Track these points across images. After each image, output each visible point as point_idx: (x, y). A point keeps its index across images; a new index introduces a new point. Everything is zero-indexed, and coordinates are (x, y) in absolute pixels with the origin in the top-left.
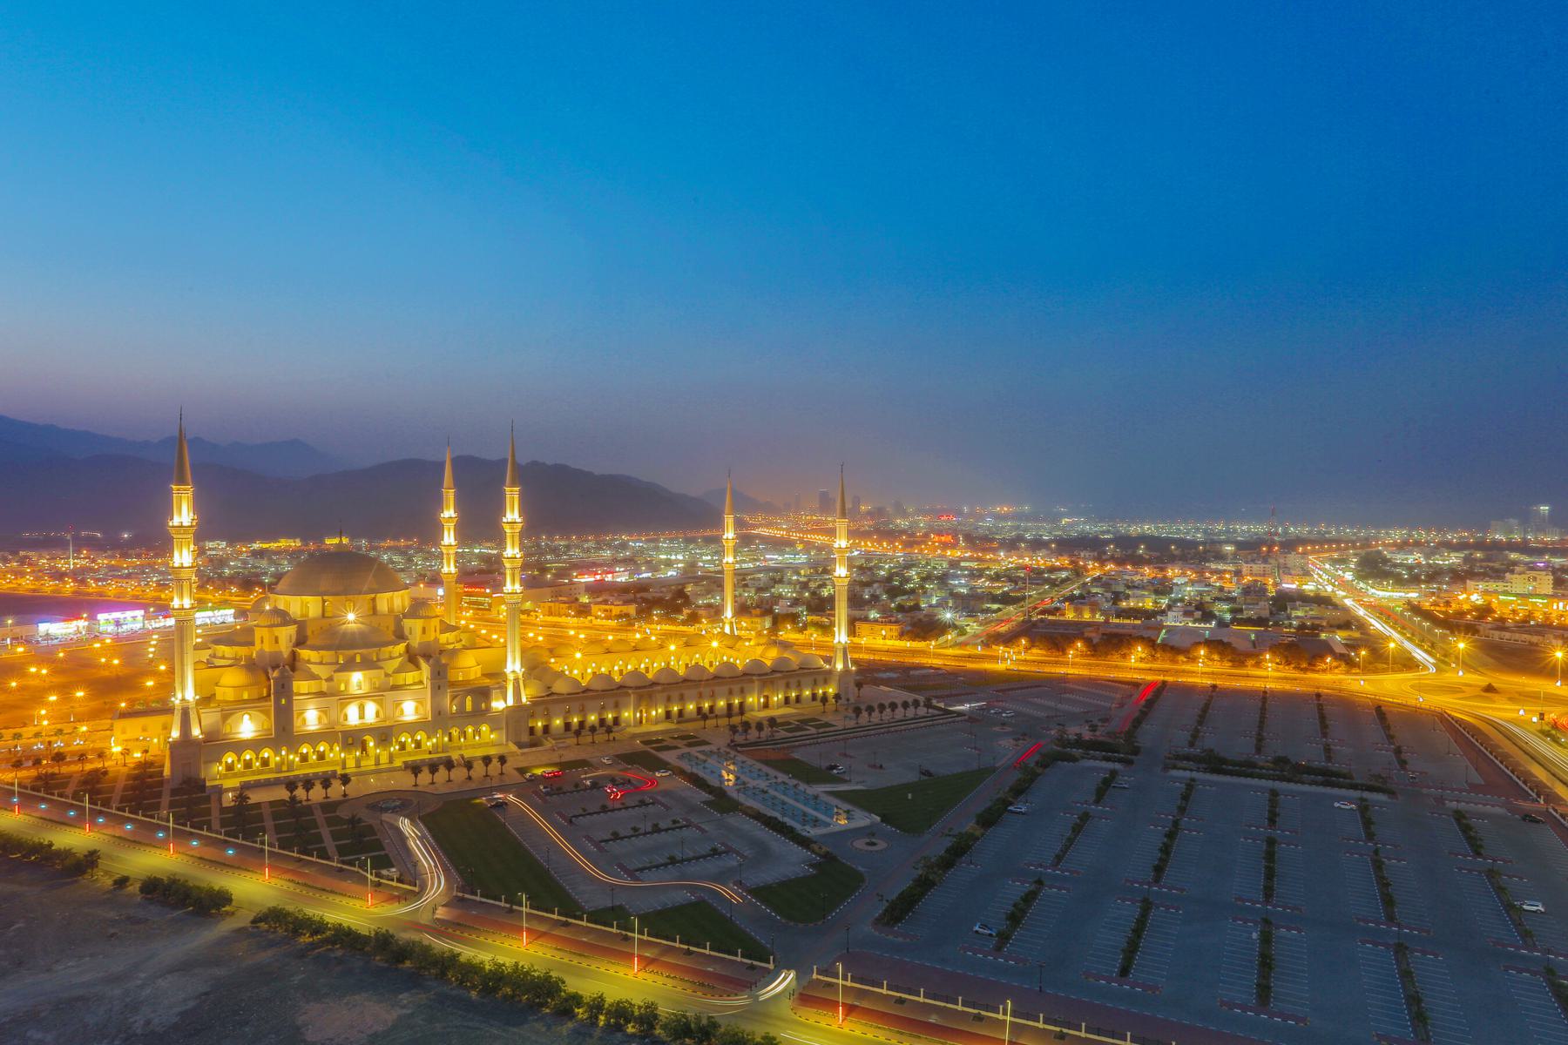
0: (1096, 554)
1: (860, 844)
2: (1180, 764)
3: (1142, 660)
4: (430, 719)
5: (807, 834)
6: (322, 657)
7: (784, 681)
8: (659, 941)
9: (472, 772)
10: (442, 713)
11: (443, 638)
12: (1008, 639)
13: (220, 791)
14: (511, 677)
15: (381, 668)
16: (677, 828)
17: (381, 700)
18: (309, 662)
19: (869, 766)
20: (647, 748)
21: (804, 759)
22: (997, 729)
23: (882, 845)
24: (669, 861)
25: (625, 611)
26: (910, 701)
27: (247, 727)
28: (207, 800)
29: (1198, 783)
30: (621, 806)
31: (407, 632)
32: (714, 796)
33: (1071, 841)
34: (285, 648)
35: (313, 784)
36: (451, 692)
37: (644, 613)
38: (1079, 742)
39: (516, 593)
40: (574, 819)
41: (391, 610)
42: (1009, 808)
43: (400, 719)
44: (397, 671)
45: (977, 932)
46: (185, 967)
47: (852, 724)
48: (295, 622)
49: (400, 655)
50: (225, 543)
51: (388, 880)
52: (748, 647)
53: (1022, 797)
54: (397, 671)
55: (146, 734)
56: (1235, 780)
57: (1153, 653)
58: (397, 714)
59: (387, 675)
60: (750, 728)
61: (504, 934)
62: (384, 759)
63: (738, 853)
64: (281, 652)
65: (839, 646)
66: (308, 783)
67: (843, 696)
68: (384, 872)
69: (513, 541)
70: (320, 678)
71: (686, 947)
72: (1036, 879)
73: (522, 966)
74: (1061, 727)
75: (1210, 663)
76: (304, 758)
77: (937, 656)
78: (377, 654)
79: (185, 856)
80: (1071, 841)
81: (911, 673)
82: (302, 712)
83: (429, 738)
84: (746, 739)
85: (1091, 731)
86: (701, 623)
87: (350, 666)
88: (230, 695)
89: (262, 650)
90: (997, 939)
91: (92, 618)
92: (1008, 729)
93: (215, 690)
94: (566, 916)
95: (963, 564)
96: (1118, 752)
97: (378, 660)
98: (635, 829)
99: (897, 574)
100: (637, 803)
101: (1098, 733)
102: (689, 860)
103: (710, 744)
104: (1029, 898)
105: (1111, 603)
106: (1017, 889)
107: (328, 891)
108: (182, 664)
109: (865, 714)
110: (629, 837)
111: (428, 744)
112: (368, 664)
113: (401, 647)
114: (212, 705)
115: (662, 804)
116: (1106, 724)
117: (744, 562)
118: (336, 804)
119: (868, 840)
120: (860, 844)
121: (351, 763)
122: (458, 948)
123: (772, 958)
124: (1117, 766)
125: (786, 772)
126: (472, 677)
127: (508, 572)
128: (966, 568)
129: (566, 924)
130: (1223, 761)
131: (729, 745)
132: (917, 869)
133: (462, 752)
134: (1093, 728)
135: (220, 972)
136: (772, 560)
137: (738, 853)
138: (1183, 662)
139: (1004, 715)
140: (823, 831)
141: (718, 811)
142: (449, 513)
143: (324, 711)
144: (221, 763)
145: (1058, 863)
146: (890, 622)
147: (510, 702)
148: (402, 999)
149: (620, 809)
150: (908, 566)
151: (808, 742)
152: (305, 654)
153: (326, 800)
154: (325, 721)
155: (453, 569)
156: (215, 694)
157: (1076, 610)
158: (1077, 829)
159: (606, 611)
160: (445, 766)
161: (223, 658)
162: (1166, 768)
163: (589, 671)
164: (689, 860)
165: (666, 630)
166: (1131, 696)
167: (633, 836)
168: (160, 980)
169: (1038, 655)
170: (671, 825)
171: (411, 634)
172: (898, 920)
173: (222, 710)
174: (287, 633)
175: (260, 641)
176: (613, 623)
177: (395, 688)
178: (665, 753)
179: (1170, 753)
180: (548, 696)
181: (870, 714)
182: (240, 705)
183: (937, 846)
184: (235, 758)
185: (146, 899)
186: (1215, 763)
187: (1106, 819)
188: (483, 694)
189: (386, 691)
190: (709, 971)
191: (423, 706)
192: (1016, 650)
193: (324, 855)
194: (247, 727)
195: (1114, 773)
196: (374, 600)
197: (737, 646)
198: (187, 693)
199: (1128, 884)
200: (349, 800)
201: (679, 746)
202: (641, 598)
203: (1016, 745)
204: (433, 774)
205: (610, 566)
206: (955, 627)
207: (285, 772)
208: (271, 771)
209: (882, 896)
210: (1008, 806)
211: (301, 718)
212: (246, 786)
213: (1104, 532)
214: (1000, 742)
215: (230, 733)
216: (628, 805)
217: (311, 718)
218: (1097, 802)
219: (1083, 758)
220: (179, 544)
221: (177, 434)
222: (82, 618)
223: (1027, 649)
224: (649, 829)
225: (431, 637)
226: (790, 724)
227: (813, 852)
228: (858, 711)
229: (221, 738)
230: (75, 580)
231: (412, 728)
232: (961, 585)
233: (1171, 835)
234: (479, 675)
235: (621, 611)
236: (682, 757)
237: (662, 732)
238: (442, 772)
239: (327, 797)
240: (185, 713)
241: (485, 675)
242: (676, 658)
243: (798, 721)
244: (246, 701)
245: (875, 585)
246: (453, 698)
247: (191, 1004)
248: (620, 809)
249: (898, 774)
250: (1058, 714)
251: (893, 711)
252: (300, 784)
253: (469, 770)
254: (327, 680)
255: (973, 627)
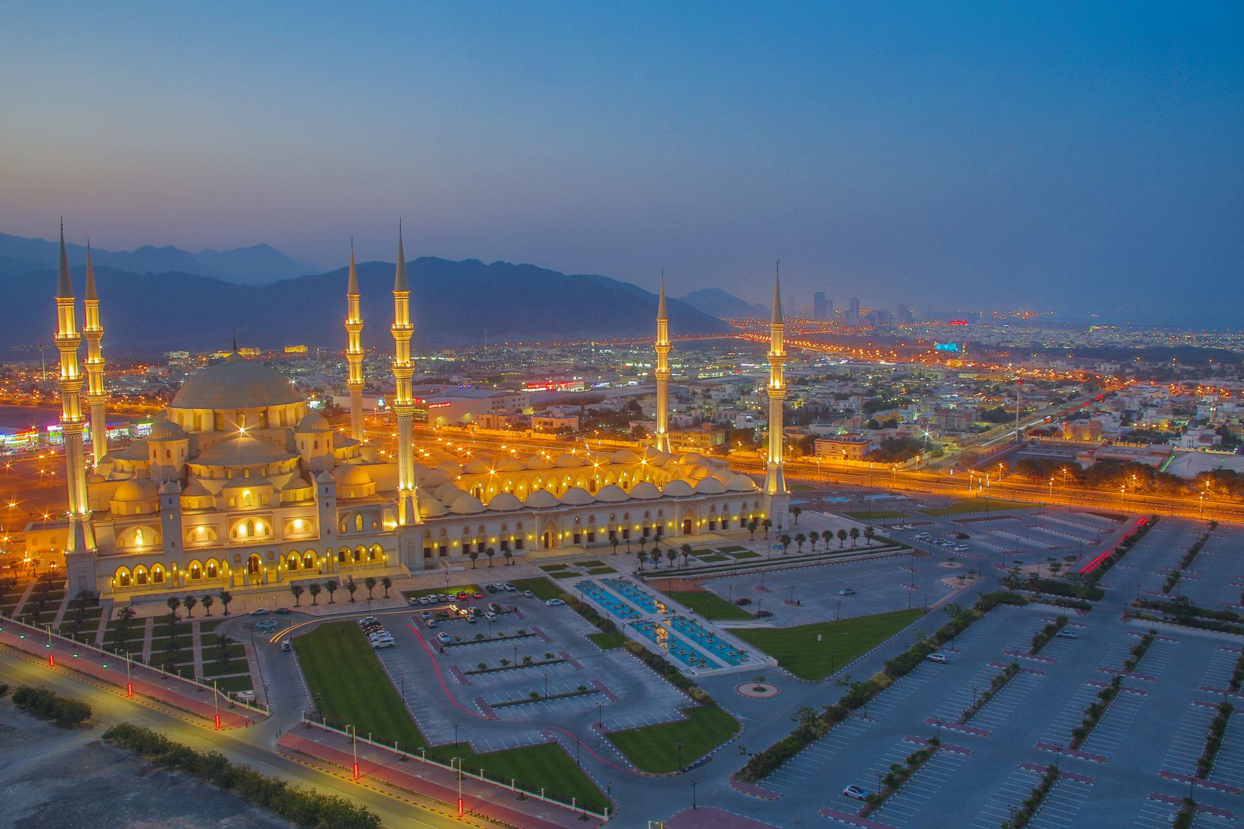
0: (1118, 367)
1: (747, 689)
2: (1144, 612)
3: (1137, 490)
4: (319, 538)
5: (692, 676)
6: (212, 472)
7: (708, 506)
8: (494, 783)
9: (355, 594)
10: (331, 531)
11: (340, 452)
12: (985, 464)
13: (113, 605)
14: (403, 495)
15: (271, 484)
16: (552, 662)
17: (271, 517)
18: (199, 476)
19: (786, 602)
20: (547, 575)
21: (715, 592)
22: (943, 564)
23: (771, 691)
24: (531, 698)
25: (567, 424)
26: (848, 531)
27: (139, 542)
28: (99, 613)
29: (1158, 635)
30: (499, 637)
31: (299, 446)
32: (602, 630)
33: (988, 696)
34: (176, 462)
35: (195, 602)
36: (339, 511)
37: (586, 428)
38: (1035, 583)
39: (407, 406)
40: (445, 648)
41: (284, 423)
42: (928, 656)
43: (290, 537)
44: (288, 487)
45: (846, 794)
46: (33, 777)
47: (780, 553)
48: (187, 435)
49: (291, 471)
50: (188, 353)
51: (242, 702)
52: (676, 465)
53: (948, 644)
54: (288, 487)
55: (56, 546)
56: (1207, 633)
57: (1151, 482)
58: (287, 531)
59: (276, 491)
60: (660, 555)
61: (339, 765)
62: (272, 578)
63: (609, 693)
64: (173, 467)
65: (774, 467)
66: (190, 602)
67: (775, 524)
68: (241, 694)
69: (403, 349)
70: (211, 494)
71: (520, 791)
72: (932, 738)
73: (341, 801)
74: (1053, 561)
75: (1219, 497)
76: (196, 574)
77: (901, 478)
78: (266, 470)
79: (63, 668)
80: (988, 696)
81: (866, 498)
82: (190, 528)
83: (318, 557)
84: (656, 568)
85: (1051, 570)
86: (645, 438)
87: (239, 480)
88: (123, 509)
89: (155, 464)
90: (866, 803)
91: (42, 429)
92: (957, 565)
93: (109, 504)
94: (405, 750)
95: (961, 376)
96: (1074, 596)
97: (267, 476)
98: (504, 662)
99: (882, 386)
100: (517, 634)
101: (1060, 573)
102: (553, 698)
103: (617, 572)
104: (916, 760)
105: (1119, 424)
106: (910, 746)
107: (183, 710)
108: (74, 479)
109: (794, 543)
110: (497, 670)
111: (318, 563)
112: (257, 479)
113: (292, 462)
114: (106, 519)
115: (544, 636)
116: (1072, 563)
117: (714, 370)
118: (217, 622)
119: (756, 685)
120: (747, 689)
121: (239, 581)
122: (284, 777)
123: (606, 809)
124: (1070, 612)
125: (688, 606)
126: (365, 494)
127: (399, 383)
128: (963, 381)
129: (405, 759)
130: (1197, 612)
131: (635, 573)
132: (795, 721)
133: (350, 573)
134: (1056, 567)
135: (65, 784)
136: (746, 368)
137: (609, 693)
138: (1186, 494)
139: (957, 549)
140: (708, 672)
141: (599, 645)
142: (354, 319)
143: (214, 527)
144: (115, 577)
145: (965, 721)
146: (855, 440)
147: (403, 522)
148: (222, 824)
149: (496, 640)
150: (897, 379)
151: (725, 572)
152: (197, 468)
153: (207, 618)
154: (215, 537)
155: (359, 380)
156: (110, 509)
157: (1074, 431)
158: (999, 683)
159: (546, 423)
160: (327, 588)
161: (122, 471)
162: (1128, 616)
163: (564, 484)
164: (553, 698)
165: (608, 445)
166: (1112, 531)
167: (501, 669)
168: (9, 788)
169: (1018, 481)
170: (544, 659)
171: (303, 448)
172: (761, 775)
173: (114, 525)
174: (178, 447)
175: (153, 456)
176: (552, 437)
177: (286, 504)
178: (564, 580)
179: (1138, 600)
180: (445, 515)
181: (800, 544)
182: (134, 520)
183: (829, 693)
184: (217, 565)
185: (19, 708)
186: (1185, 614)
187: (1038, 673)
188: (376, 514)
189: (275, 507)
190: (539, 820)
191: (312, 523)
192: (994, 475)
193: (189, 673)
194: (139, 542)
195: (1062, 621)
196: (265, 412)
197: (667, 465)
198: (81, 507)
199: (1041, 749)
200: (229, 619)
201: (581, 573)
202: (590, 410)
203: (962, 584)
204: (315, 596)
205: (566, 376)
206: (929, 447)
207: (176, 588)
208: (164, 587)
209: (744, 749)
210: (928, 653)
211: (190, 534)
212: (135, 601)
213: (1136, 342)
214: (942, 580)
215: (124, 548)
216: (506, 635)
217: (201, 533)
218: (1034, 653)
219: (1033, 601)
220: (66, 356)
221: (59, 240)
222: (31, 430)
223: (1006, 474)
224: (520, 662)
225: (324, 451)
226: (709, 551)
227: (692, 696)
228: (786, 540)
229: (115, 552)
230: (42, 392)
231: (301, 546)
232: (952, 400)
233: (1107, 696)
234: (373, 492)
235: (562, 424)
236: (579, 586)
237: (567, 558)
238: (324, 595)
239: (209, 615)
240: (79, 526)
241: (380, 493)
242: (602, 477)
243: (718, 549)
244: (137, 516)
245: (851, 399)
246: (342, 517)
247: (31, 813)
248: (496, 640)
249: (812, 613)
250: (1020, 549)
251: (827, 540)
252: (199, 600)
253: (352, 592)
254: (216, 496)
255: (951, 448)
